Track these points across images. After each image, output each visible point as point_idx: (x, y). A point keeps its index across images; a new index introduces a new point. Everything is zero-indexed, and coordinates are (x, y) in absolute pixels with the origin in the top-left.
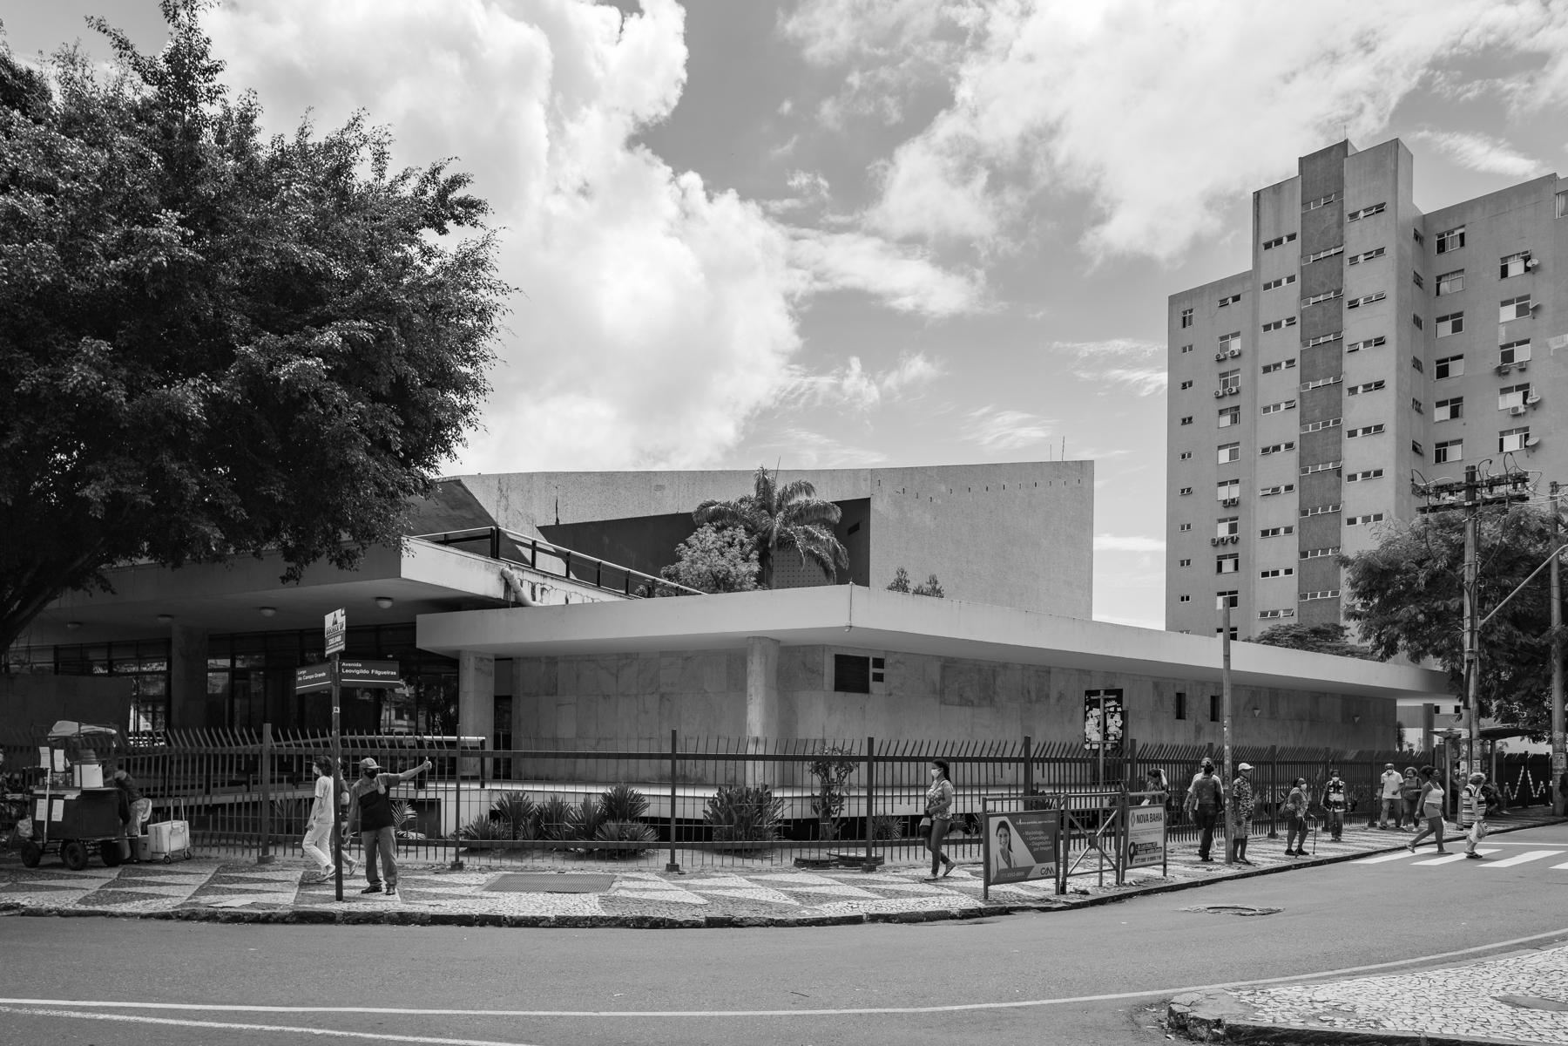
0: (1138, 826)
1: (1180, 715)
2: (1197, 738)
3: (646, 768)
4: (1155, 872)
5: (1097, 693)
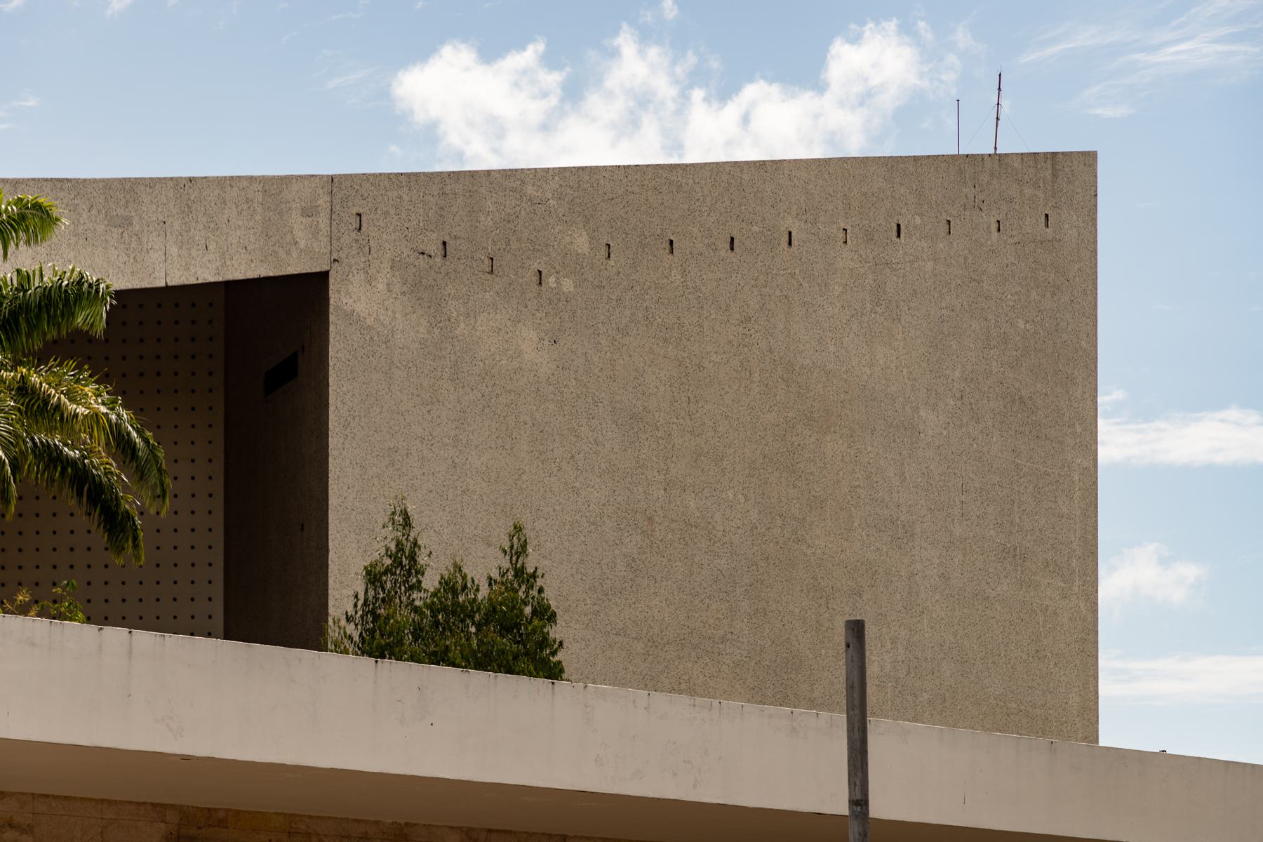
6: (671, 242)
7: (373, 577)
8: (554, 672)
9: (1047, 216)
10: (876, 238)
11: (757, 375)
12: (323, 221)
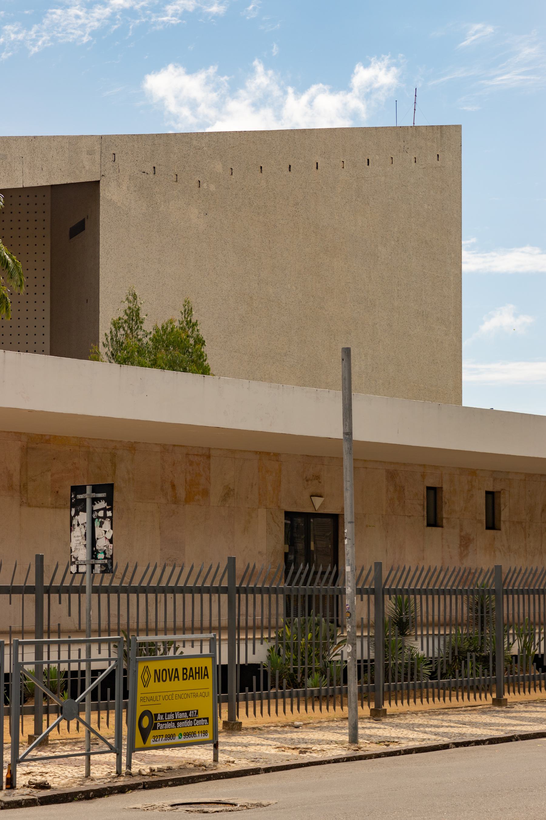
0: (154, 686)
1: (434, 521)
2: (462, 556)
3: (173, 607)
4: (202, 754)
5: (81, 489)
6: (261, 167)
7: (117, 325)
8: (205, 371)
9: (438, 155)
10: (357, 165)
11: (301, 230)
12: (97, 157)
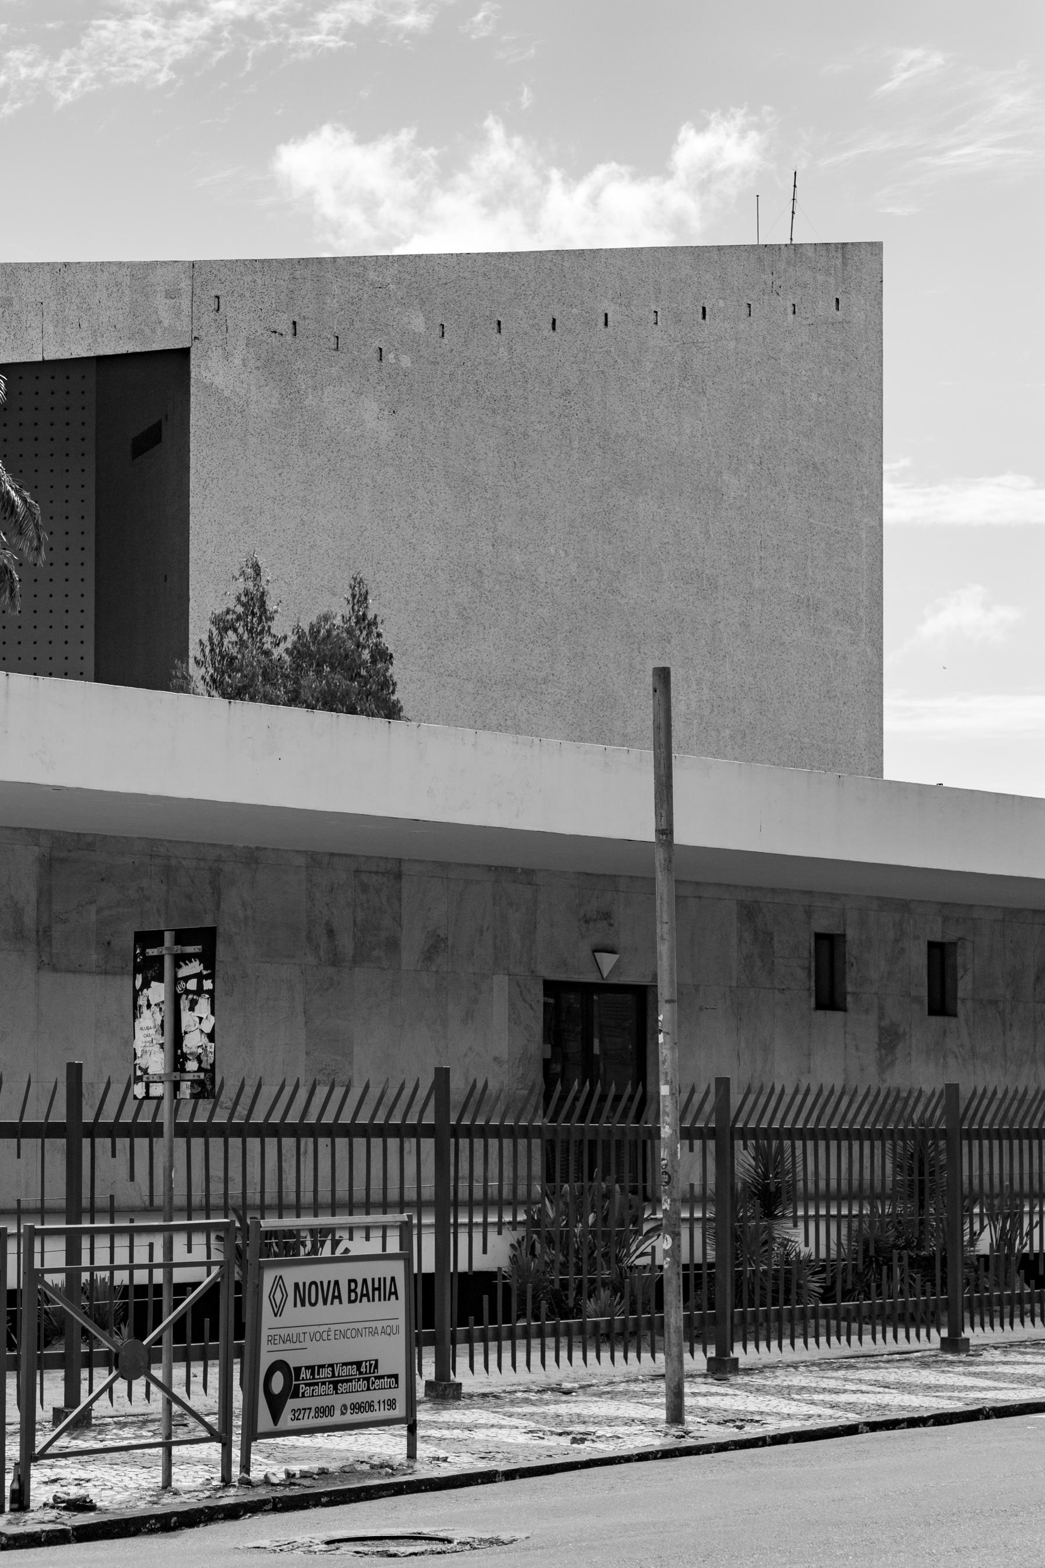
0: (295, 1315)
1: (829, 998)
2: (884, 1066)
3: (329, 1164)
4: (385, 1445)
5: (155, 938)
